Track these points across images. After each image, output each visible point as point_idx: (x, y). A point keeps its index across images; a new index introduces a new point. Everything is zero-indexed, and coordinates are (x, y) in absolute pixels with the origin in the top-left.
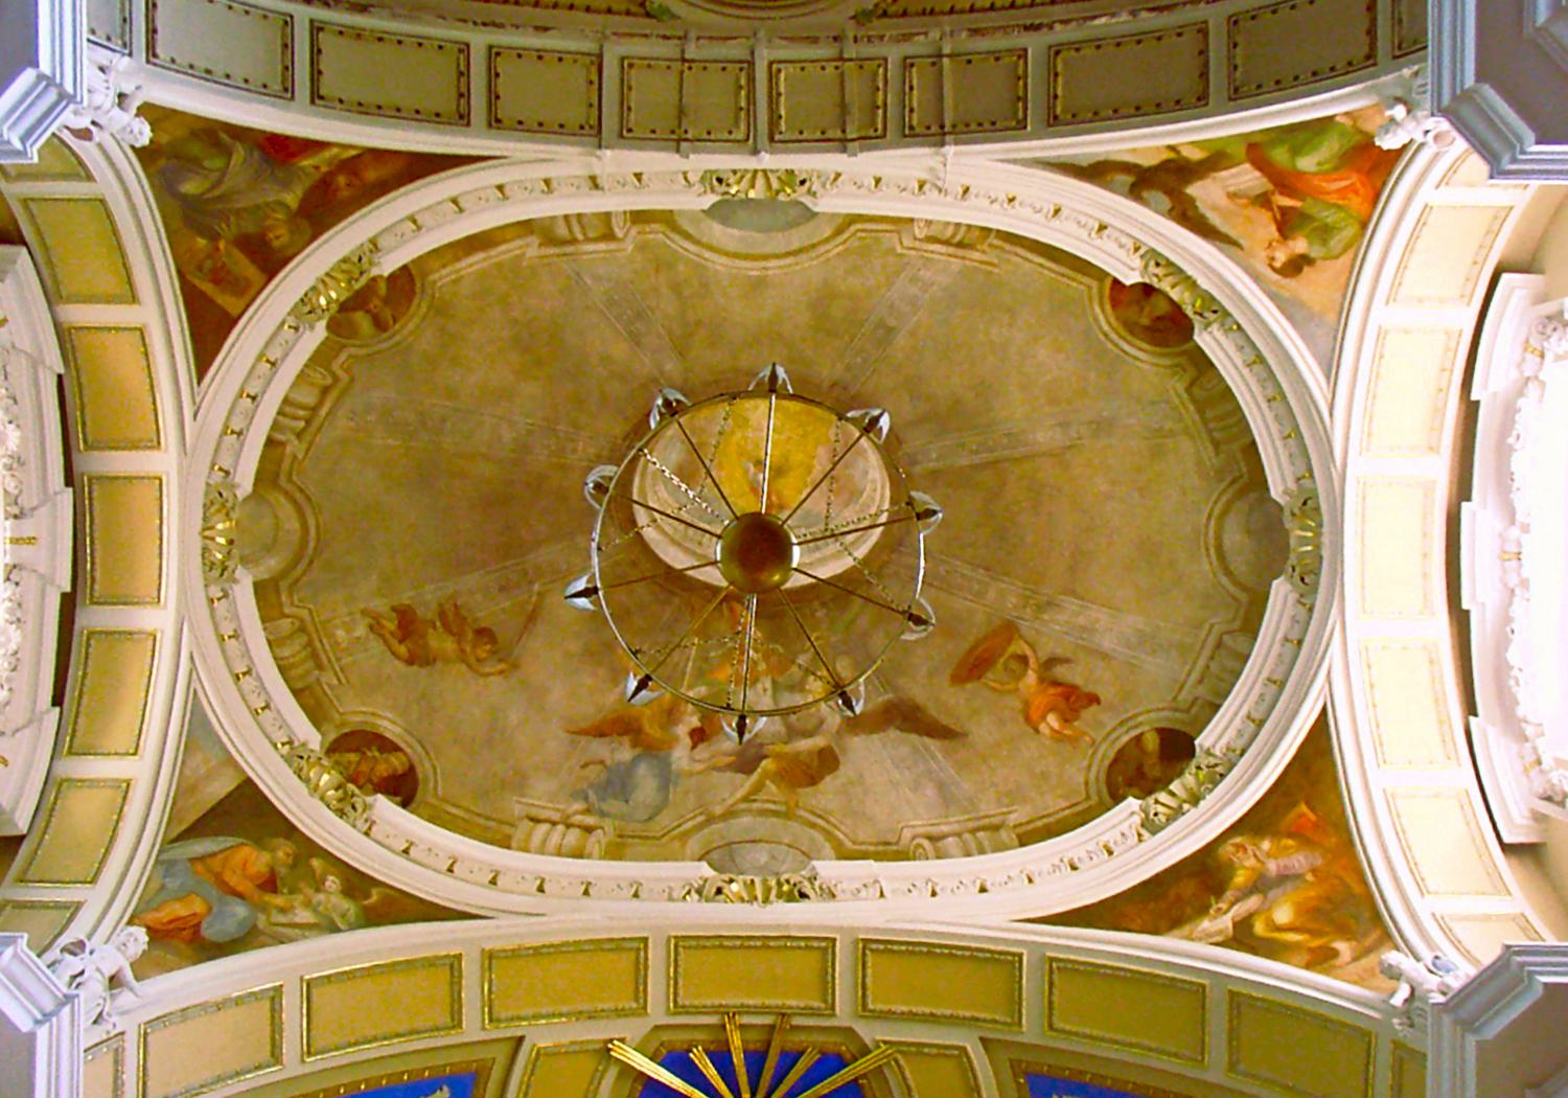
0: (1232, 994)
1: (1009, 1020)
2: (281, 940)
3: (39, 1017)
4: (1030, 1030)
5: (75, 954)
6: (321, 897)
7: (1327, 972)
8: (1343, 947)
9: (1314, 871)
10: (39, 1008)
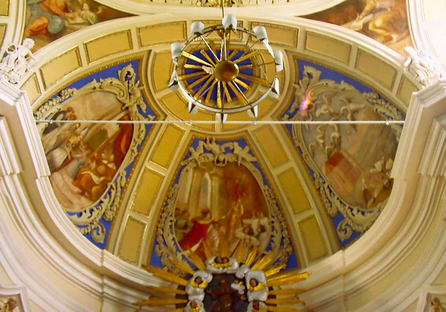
0: (359, 49)
1: (293, 45)
2: (74, 30)
3: (15, 100)
4: (299, 49)
5: (12, 51)
6: (83, 12)
7: (388, 46)
8: (395, 37)
9: (391, 8)
10: (14, 97)
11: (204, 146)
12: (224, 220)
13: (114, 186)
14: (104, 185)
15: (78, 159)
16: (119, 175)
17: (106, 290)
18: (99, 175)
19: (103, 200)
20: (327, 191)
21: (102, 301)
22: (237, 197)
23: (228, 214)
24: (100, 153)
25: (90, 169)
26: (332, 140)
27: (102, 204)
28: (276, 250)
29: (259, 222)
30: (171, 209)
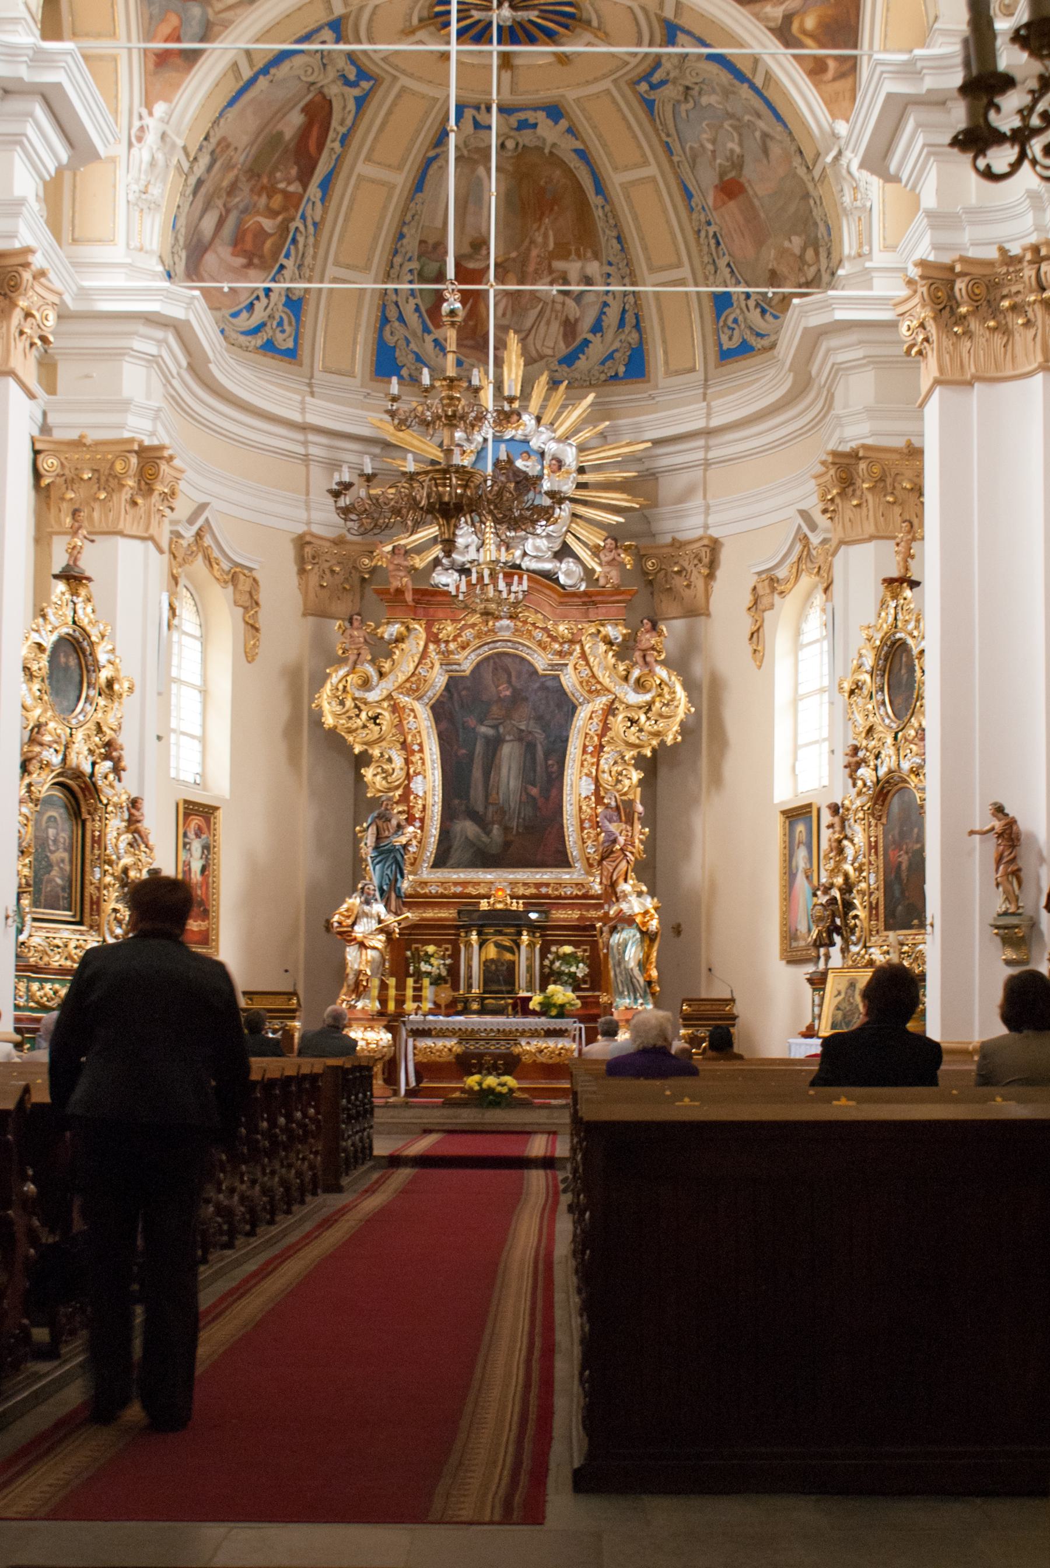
11: (474, 118)
12: (514, 260)
13: (302, 228)
14: (284, 228)
15: (236, 206)
16: (309, 199)
17: (313, 450)
18: (272, 213)
19: (285, 262)
20: (713, 242)
21: (307, 466)
22: (543, 214)
23: (523, 248)
24: (271, 175)
25: (258, 213)
26: (728, 153)
27: (284, 272)
28: (610, 334)
29: (582, 268)
30: (410, 244)
